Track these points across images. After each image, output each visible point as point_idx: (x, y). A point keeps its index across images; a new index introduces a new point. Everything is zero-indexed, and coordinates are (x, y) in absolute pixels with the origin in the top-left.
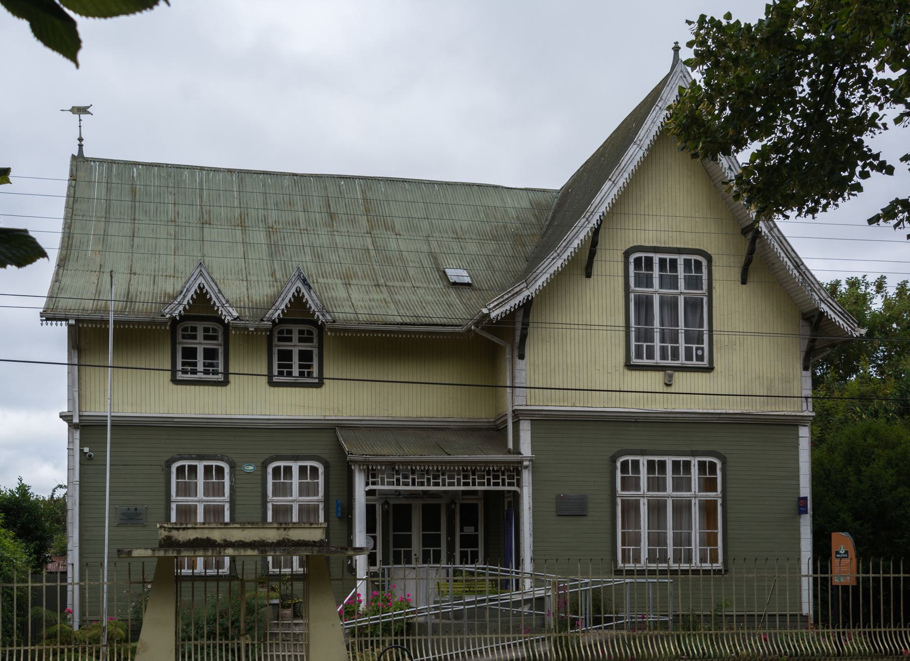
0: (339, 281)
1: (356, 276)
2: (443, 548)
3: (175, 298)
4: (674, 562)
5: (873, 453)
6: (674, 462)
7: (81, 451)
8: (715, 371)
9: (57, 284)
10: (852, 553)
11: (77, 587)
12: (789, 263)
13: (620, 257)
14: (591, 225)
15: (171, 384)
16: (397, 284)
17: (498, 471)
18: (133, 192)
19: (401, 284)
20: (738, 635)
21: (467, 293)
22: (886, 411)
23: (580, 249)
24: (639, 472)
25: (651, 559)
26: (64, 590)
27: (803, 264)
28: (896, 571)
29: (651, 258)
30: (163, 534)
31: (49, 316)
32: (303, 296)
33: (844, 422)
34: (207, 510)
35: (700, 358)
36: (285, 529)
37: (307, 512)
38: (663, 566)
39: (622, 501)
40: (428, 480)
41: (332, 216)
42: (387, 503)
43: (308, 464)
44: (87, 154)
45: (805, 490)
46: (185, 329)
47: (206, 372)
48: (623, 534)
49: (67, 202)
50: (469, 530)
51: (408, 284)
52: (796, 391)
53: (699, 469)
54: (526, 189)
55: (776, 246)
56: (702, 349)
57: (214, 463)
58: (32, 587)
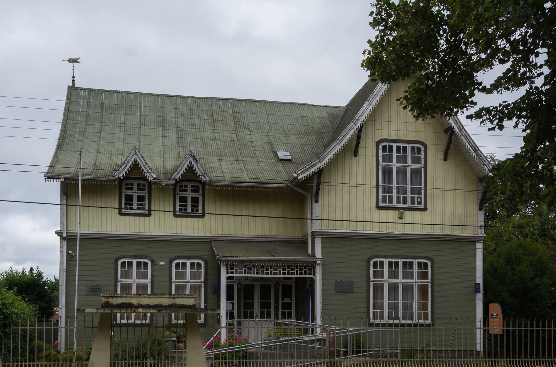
0: (216, 158)
1: (226, 155)
2: (272, 310)
3: (121, 166)
4: (403, 319)
5: (522, 258)
6: (403, 262)
7: (67, 253)
8: (428, 210)
9: (56, 158)
10: (501, 316)
11: (63, 330)
12: (471, 149)
13: (374, 145)
14: (356, 127)
15: (118, 215)
16: (249, 159)
17: (302, 266)
18: (102, 107)
19: (251, 160)
20: (433, 361)
21: (289, 165)
22: (533, 234)
23: (350, 140)
24: (383, 268)
25: (389, 318)
26: (56, 331)
27: (479, 149)
28: (550, 326)
29: (392, 146)
30: (104, 300)
31: (49, 176)
32: (193, 166)
33: (509, 240)
34: (138, 287)
35: (419, 203)
36: (173, 298)
37: (195, 288)
38: (396, 322)
39: (374, 284)
40: (263, 271)
41: (214, 121)
42: (240, 284)
43: (196, 261)
44: (77, 85)
45: (479, 279)
46: (127, 184)
47: (138, 209)
48: (374, 303)
49: (64, 113)
50: (287, 300)
51: (255, 160)
52: (474, 222)
53: (418, 266)
54: (326, 106)
55: (464, 139)
56: (421, 198)
57: (142, 260)
58: (30, 329)
